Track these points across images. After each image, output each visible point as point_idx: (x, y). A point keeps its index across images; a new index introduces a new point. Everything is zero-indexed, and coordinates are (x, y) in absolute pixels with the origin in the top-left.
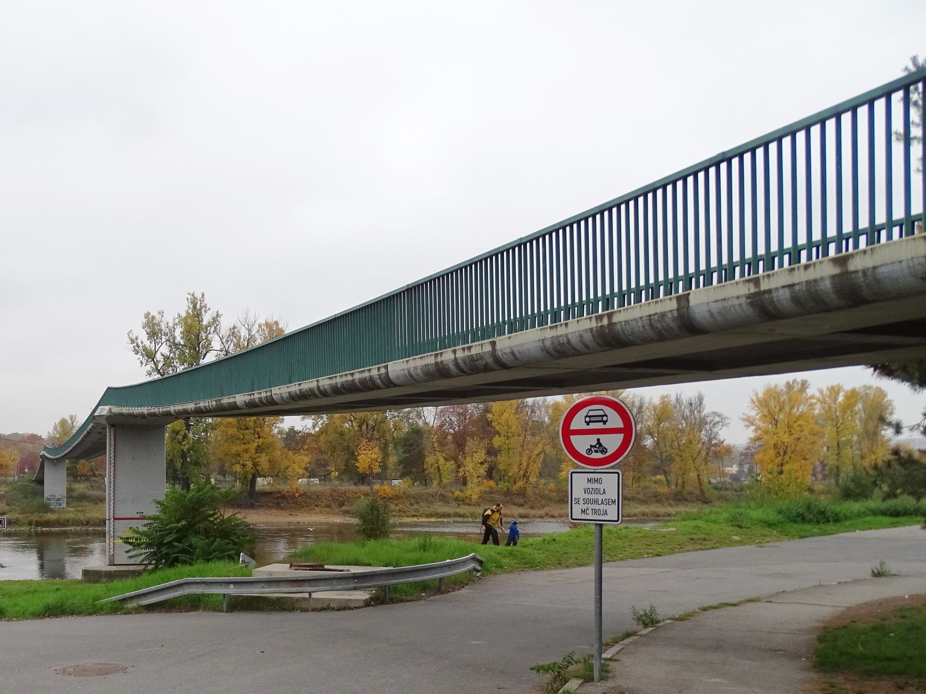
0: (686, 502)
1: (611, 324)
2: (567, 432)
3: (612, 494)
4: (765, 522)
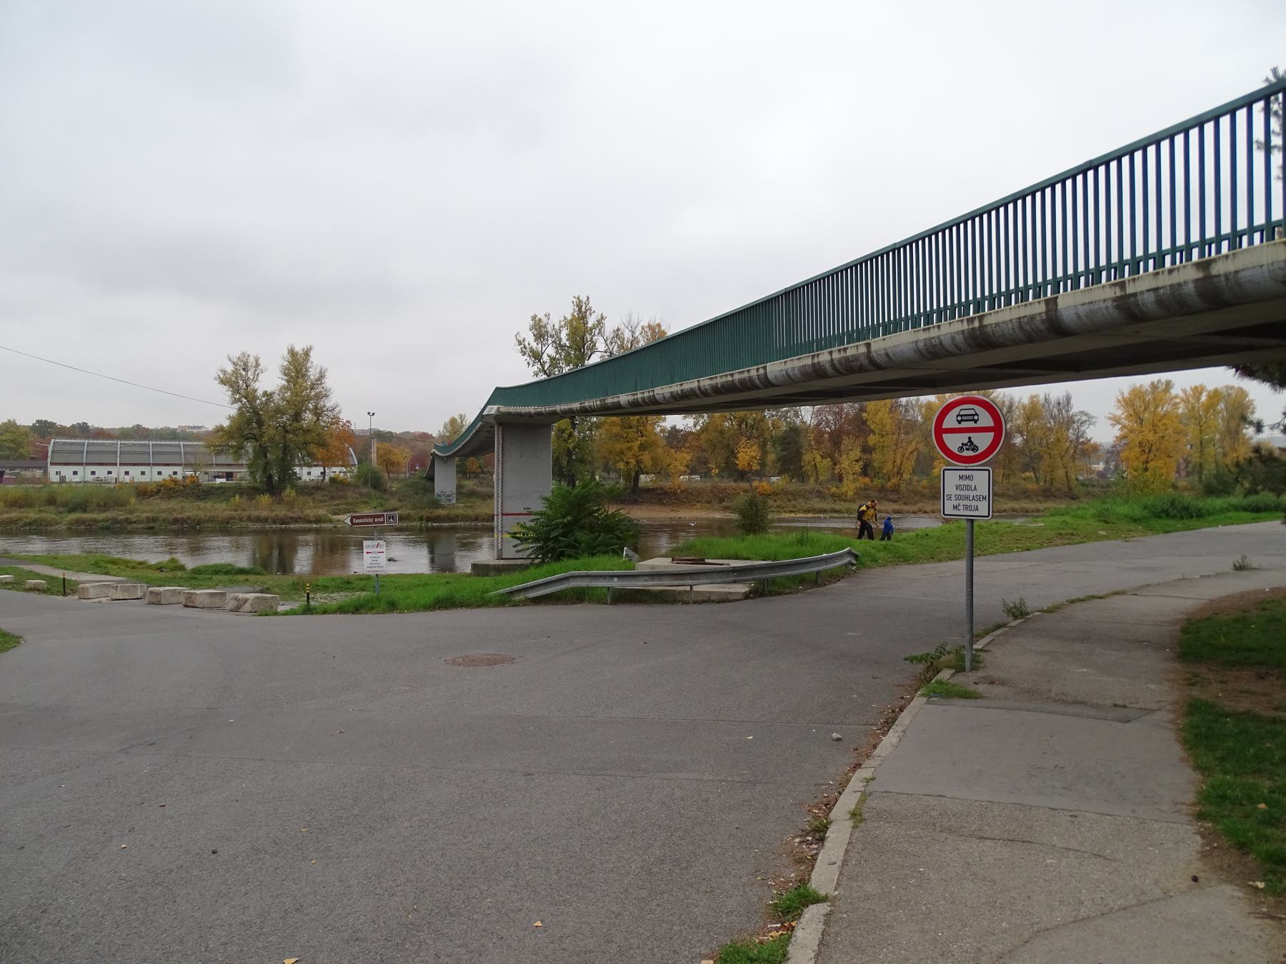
0: (1054, 499)
1: (982, 327)
2: (940, 431)
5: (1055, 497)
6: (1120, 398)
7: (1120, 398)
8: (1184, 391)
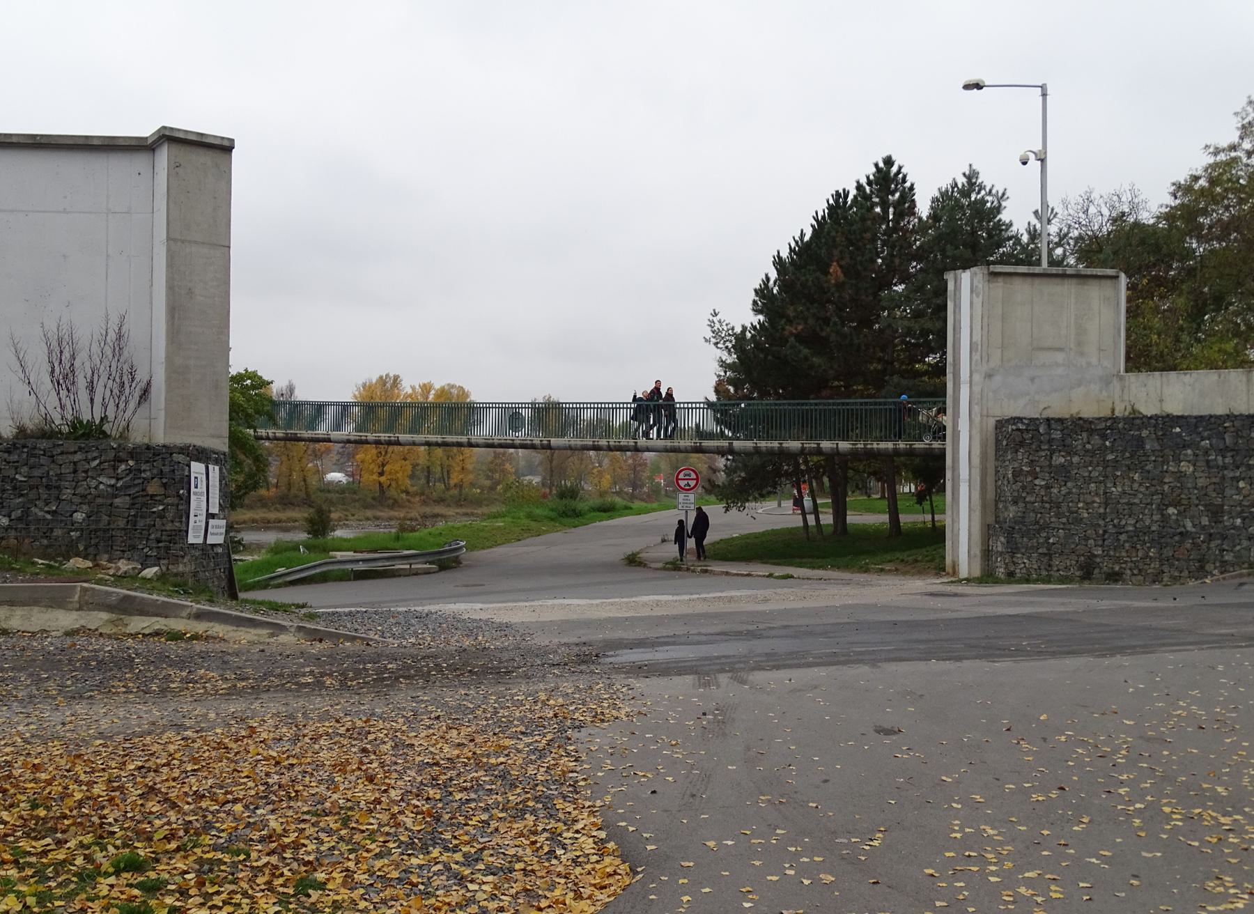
0: (292, 507)
1: (700, 446)
2: (678, 479)
4: (549, 518)
5: (292, 504)
6: (357, 393)
7: (357, 393)
8: (413, 388)
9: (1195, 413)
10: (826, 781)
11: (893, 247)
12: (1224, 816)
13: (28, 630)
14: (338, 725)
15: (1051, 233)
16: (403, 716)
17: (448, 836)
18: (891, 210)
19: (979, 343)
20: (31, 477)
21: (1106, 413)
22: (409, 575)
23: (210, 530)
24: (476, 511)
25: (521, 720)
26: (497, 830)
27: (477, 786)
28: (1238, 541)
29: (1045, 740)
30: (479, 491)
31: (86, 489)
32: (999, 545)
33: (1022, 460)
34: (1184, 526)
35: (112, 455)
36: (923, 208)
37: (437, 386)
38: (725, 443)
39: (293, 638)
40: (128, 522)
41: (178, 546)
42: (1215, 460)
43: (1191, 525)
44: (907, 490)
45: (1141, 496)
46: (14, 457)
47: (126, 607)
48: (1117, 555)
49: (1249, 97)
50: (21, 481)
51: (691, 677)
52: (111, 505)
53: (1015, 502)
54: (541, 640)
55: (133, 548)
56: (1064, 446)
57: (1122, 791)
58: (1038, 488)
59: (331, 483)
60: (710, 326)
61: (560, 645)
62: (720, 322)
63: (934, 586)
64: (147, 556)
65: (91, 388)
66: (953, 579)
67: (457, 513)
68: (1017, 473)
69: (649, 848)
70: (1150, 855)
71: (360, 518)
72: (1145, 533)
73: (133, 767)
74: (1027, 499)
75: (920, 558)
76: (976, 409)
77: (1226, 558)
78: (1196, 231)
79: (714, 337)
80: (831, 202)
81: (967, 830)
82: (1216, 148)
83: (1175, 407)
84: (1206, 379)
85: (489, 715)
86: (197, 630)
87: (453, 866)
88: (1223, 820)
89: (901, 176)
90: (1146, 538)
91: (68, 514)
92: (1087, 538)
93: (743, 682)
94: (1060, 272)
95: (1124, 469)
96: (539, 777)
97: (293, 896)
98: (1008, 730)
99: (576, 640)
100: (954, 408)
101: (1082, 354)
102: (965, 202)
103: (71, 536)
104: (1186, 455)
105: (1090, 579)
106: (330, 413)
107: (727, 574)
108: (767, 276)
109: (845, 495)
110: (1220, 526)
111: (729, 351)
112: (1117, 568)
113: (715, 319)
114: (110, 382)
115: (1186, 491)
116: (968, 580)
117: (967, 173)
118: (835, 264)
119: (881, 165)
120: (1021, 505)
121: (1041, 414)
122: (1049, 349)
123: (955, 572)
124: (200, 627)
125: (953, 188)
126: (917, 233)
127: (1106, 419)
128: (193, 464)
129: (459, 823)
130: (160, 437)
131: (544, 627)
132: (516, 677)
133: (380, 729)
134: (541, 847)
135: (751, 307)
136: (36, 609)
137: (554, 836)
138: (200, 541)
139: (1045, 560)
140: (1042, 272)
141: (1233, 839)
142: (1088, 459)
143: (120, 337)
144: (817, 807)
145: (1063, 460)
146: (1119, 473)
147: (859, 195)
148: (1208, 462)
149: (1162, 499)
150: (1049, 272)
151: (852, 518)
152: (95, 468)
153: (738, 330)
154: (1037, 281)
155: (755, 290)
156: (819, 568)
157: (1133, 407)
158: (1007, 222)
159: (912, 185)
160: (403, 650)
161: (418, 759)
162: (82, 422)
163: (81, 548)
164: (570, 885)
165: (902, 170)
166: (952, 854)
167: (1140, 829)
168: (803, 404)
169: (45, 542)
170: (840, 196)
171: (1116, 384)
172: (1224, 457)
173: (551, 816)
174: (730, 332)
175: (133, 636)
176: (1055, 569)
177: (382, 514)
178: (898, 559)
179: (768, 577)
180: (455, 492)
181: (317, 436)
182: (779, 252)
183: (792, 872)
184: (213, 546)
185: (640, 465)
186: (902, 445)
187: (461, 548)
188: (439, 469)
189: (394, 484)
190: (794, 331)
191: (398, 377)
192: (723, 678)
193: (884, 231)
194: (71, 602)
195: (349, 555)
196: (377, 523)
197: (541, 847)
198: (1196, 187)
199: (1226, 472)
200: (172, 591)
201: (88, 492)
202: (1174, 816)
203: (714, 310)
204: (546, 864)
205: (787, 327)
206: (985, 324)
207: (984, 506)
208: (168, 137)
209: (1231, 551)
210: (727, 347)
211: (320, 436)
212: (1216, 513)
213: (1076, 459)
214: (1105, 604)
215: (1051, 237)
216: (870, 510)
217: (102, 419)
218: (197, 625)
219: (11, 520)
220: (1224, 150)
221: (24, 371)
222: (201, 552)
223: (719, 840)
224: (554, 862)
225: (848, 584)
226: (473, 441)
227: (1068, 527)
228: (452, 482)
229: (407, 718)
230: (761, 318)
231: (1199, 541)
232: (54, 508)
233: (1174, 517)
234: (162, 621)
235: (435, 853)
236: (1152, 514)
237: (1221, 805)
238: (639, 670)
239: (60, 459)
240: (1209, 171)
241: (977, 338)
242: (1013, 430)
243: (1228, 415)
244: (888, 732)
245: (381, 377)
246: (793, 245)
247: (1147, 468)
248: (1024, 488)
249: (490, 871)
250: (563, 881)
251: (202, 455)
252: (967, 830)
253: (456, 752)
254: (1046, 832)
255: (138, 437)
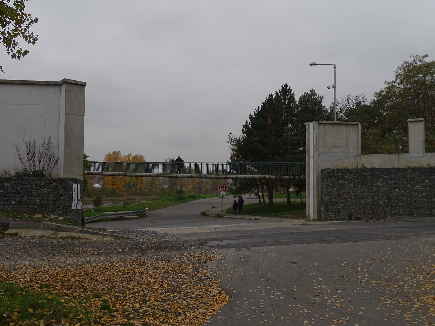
1: (227, 177)
2: (219, 188)
3: (224, 194)
8: (125, 156)
9: (383, 167)
10: (279, 275)
11: (288, 113)
12: (386, 282)
13: (27, 236)
14: (136, 262)
15: (338, 108)
16: (154, 260)
17: (178, 290)
18: (287, 101)
19: (316, 145)
20: (22, 188)
21: (355, 167)
22: (129, 219)
23: (78, 205)
24: (146, 198)
25: (188, 260)
26: (190, 288)
27: (181, 277)
28: (396, 207)
29: (338, 265)
30: (147, 191)
31: (40, 192)
32: (323, 209)
33: (330, 182)
34: (380, 203)
35: (48, 181)
36: (297, 100)
37: (133, 155)
38: (235, 176)
39: (110, 238)
40: (53, 202)
41: (69, 210)
42: (389, 182)
43: (382, 202)
44: (291, 190)
45: (366, 193)
46: (17, 182)
47: (57, 229)
48: (359, 212)
49: (398, 66)
50: (19, 190)
51: (234, 249)
52: (48, 197)
53: (328, 195)
54: (185, 239)
55: (55, 211)
56: (343, 177)
57: (359, 277)
58: (335, 191)
59: (96, 188)
60: (229, 137)
61: (192, 240)
62: (232, 136)
63: (303, 222)
64: (59, 213)
65: (40, 160)
66: (308, 220)
67: (139, 198)
68: (328, 186)
69: (234, 292)
70: (366, 292)
71: (106, 200)
72: (368, 205)
73: (84, 273)
74: (331, 194)
75: (298, 213)
76: (315, 166)
77: (393, 213)
78: (382, 108)
79: (230, 141)
80: (268, 98)
81: (318, 287)
82: (389, 82)
83: (376, 166)
84: (386, 156)
85: (178, 259)
86: (80, 236)
87: (182, 297)
88: (386, 284)
89: (290, 90)
90: (368, 206)
91: (34, 200)
92: (350, 207)
93: (250, 250)
94: (341, 123)
95: (361, 185)
96: (198, 275)
97: (142, 303)
98: (328, 262)
99: (195, 238)
100: (308, 165)
101: (347, 149)
102: (310, 99)
103: (35, 207)
104: (380, 180)
105: (351, 219)
106: (95, 165)
107: (236, 218)
108: (247, 121)
109: (273, 192)
110: (391, 202)
111: (235, 145)
112: (359, 216)
113: (230, 135)
114: (45, 158)
115: (380, 192)
116: (313, 220)
117: (311, 90)
118: (269, 118)
119: (284, 87)
120: (329, 196)
121: (335, 167)
122: (338, 147)
123: (309, 217)
124: (81, 235)
125: (306, 94)
126: (295, 108)
127: (355, 169)
128: (74, 184)
129: (180, 287)
130: (62, 176)
131: (185, 235)
132: (182, 249)
133: (148, 264)
134: (204, 292)
135: (242, 131)
136: (29, 230)
137: (207, 290)
138: (75, 208)
139: (337, 213)
140: (335, 123)
141: (388, 288)
142: (350, 182)
143: (49, 144)
144: (277, 282)
145: (342, 182)
146: (359, 186)
147: (277, 96)
148: (386, 182)
149: (373, 194)
150: (337, 123)
151: (275, 200)
152: (43, 185)
153: (238, 139)
154: (333, 126)
155: (243, 126)
156: (265, 216)
157: (363, 165)
158: (324, 106)
159: (294, 93)
160: (144, 242)
161: (163, 271)
162: (36, 171)
163: (38, 210)
164: (214, 301)
165: (290, 88)
166: (314, 292)
167: (364, 286)
168: (260, 163)
169: (27, 209)
170: (270, 96)
171: (358, 158)
172: (391, 181)
173: (205, 285)
174: (235, 139)
175: (61, 238)
176: (340, 216)
177: (114, 199)
178: (291, 213)
179: (249, 219)
180: (139, 191)
181: (99, 173)
182: (251, 114)
183: (273, 297)
184: (78, 210)
185: (202, 182)
186: (291, 177)
187: (146, 210)
188: (133, 183)
189: (118, 188)
190: (256, 140)
191: (120, 152)
192: (244, 249)
193: (285, 107)
194: (41, 228)
195: (109, 213)
196: (112, 202)
197: (204, 292)
198: (383, 94)
199: (392, 186)
200: (69, 224)
201: (41, 193)
202: (373, 283)
203: (230, 132)
204: (206, 296)
205: (254, 138)
206: (317, 139)
207: (318, 196)
208: (66, 82)
209: (394, 210)
210: (234, 144)
211: (100, 173)
212: (389, 198)
213: (346, 182)
214: (356, 227)
215: (338, 110)
216: (280, 197)
217: (43, 170)
218: (80, 235)
219: (16, 202)
220: (391, 83)
221: (19, 155)
222: (75, 212)
223: (252, 290)
224: (208, 296)
225: (276, 221)
226: (151, 175)
227: (344, 203)
228: (138, 188)
229: (155, 260)
230: (245, 135)
231: (384, 207)
232: (30, 198)
233: (376, 200)
234: (69, 233)
235: (176, 294)
236: (370, 199)
237: (385, 280)
238: (218, 247)
239: (32, 183)
240: (386, 89)
241: (315, 143)
242: (327, 172)
243: (392, 168)
244: (294, 263)
245: (114, 152)
246: (256, 111)
247: (368, 184)
248: (330, 191)
249: (192, 298)
250: (212, 300)
251: (76, 181)
252: (318, 287)
253: (173, 269)
254: (339, 287)
255: (54, 176)
